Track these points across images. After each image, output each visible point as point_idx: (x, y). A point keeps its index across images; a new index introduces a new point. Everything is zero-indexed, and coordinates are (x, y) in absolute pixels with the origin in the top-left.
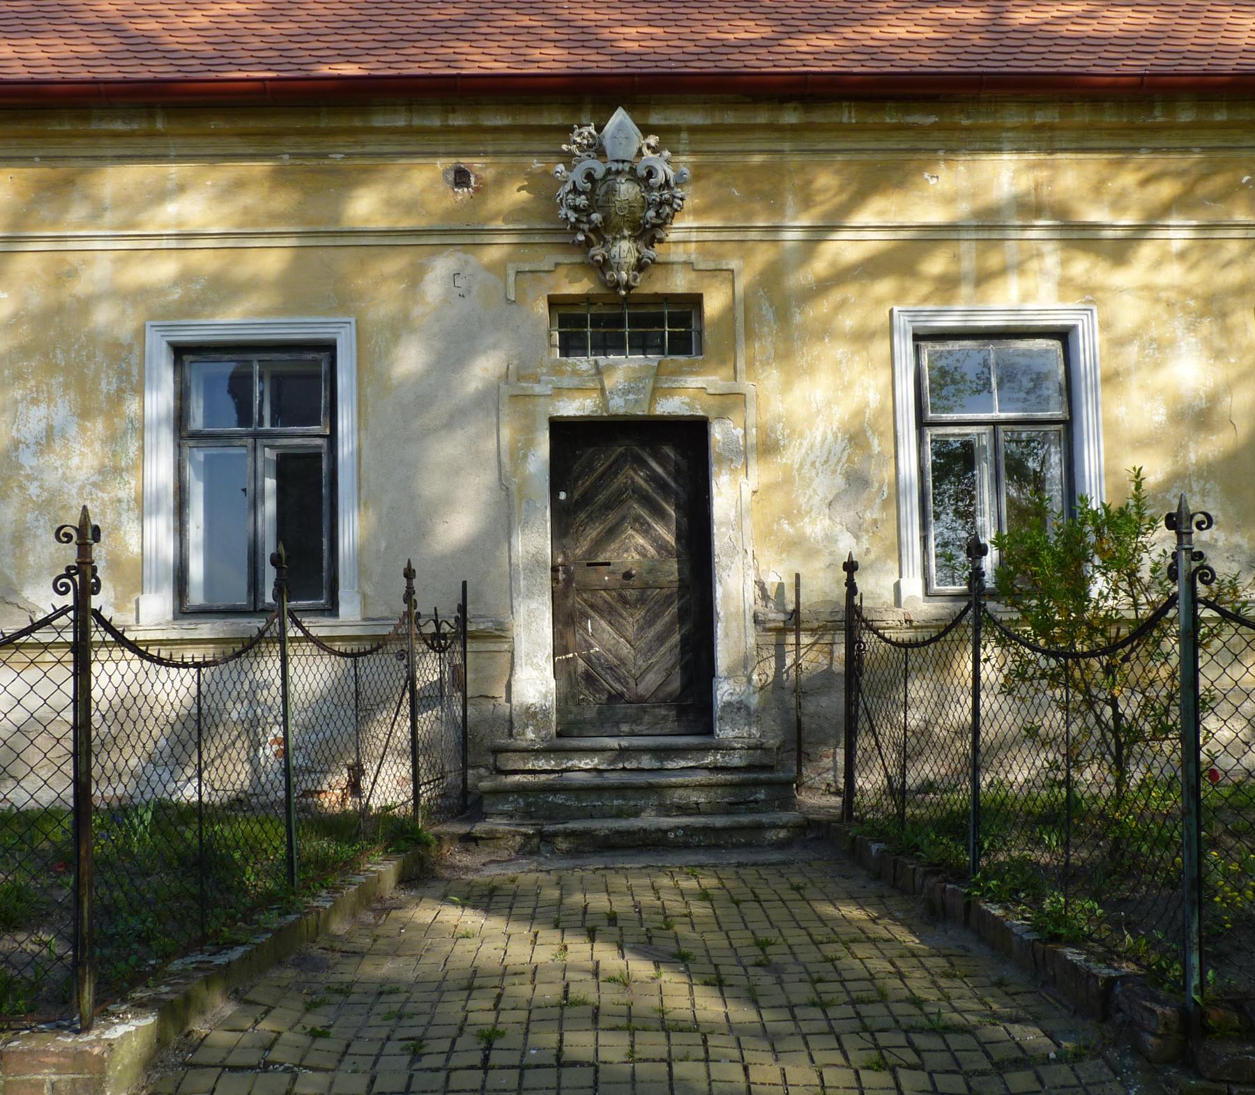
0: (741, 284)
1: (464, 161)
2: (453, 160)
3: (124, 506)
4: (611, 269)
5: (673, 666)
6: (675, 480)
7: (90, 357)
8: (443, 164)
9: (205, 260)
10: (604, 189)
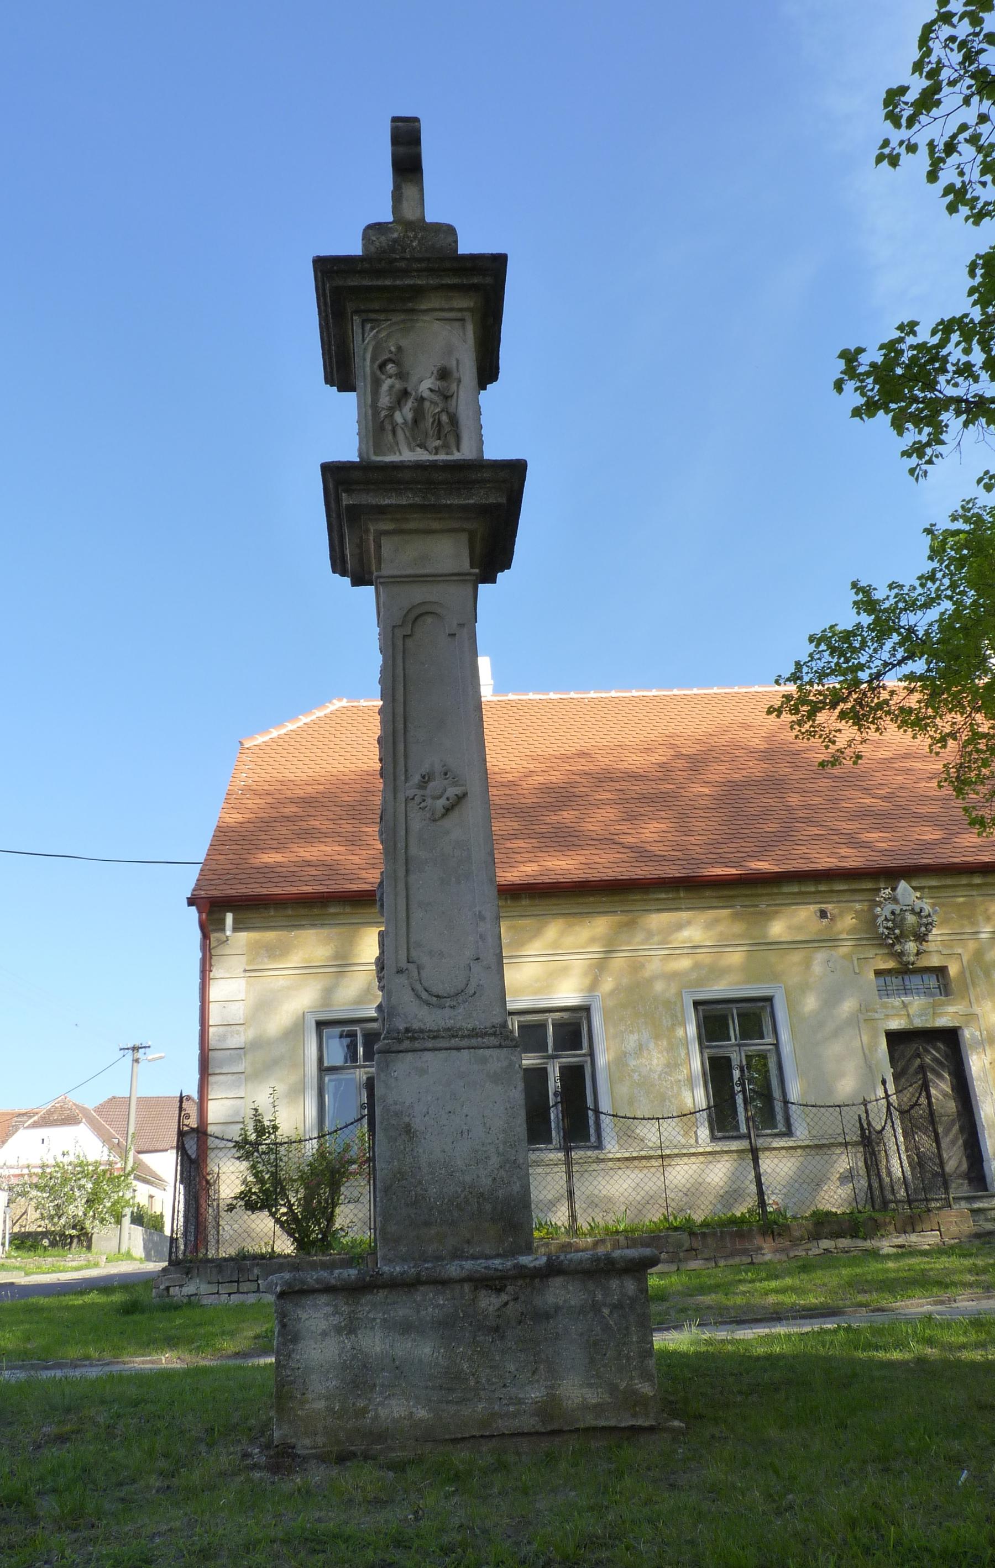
0: (965, 959)
1: (823, 906)
2: (819, 906)
3: (682, 1083)
4: (904, 955)
5: (962, 1157)
6: (946, 1060)
7: (656, 1008)
8: (816, 907)
9: (704, 958)
10: (899, 918)
